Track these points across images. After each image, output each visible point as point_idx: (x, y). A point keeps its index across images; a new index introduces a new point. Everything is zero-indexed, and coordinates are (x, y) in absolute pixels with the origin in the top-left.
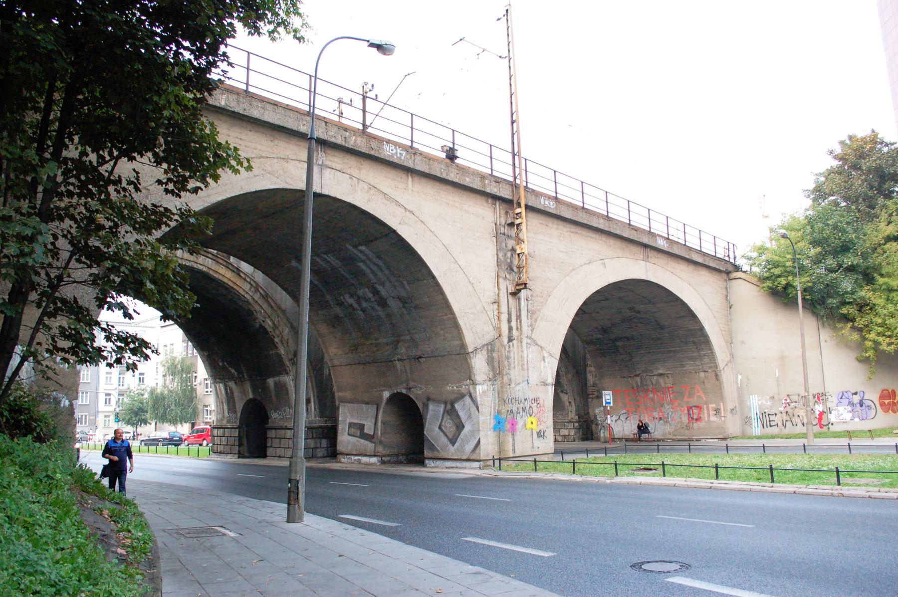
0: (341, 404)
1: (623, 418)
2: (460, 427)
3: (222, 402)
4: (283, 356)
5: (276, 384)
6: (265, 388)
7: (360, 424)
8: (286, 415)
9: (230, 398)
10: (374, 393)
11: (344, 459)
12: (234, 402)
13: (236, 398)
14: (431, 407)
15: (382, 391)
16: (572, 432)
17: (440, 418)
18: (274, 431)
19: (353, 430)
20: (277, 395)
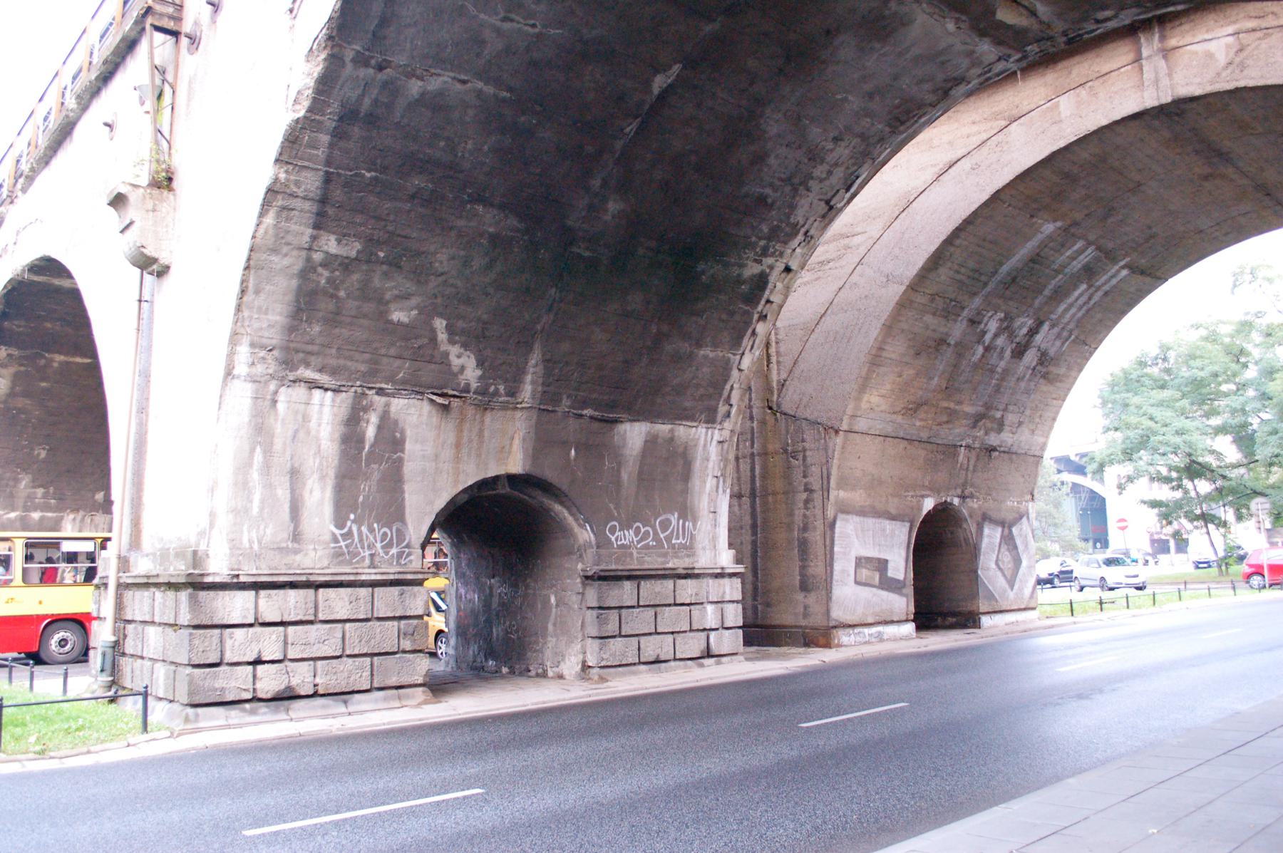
0: (840, 516)
2: (1017, 561)
3: (295, 474)
4: (735, 373)
5: (651, 443)
7: (879, 560)
8: (668, 539)
10: (909, 499)
11: (844, 637)
12: (394, 481)
14: (986, 531)
15: (923, 496)
17: (997, 548)
18: (628, 585)
19: (865, 573)
20: (645, 478)
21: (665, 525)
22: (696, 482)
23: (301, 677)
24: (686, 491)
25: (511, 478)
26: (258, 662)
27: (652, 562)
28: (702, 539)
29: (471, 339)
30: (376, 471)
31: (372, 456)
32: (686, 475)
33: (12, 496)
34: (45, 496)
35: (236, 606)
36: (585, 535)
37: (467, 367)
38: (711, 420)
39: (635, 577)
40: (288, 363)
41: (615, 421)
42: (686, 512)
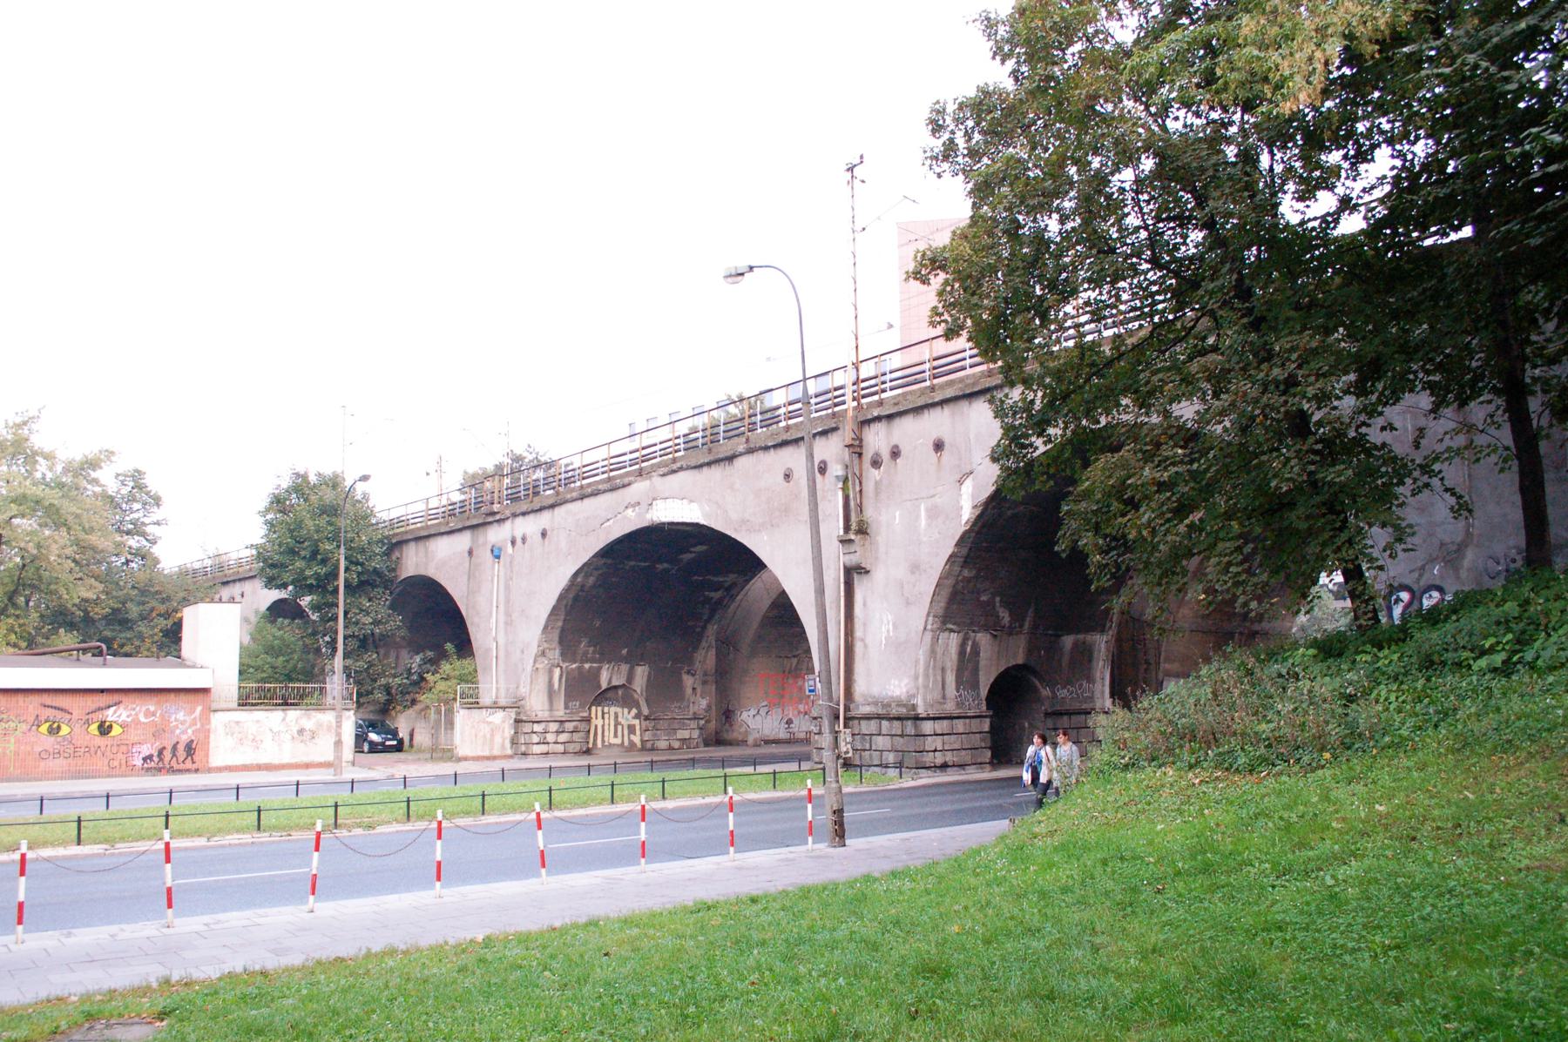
1: (763, 712)
3: (943, 670)
5: (1075, 644)
6: (1053, 648)
9: (967, 663)
12: (976, 670)
13: (982, 663)
16: (696, 734)
18: (1065, 718)
21: (1081, 685)
22: (1094, 663)
23: (949, 758)
24: (1090, 669)
25: (1017, 667)
26: (935, 751)
27: (1076, 706)
28: (1097, 694)
29: (1006, 604)
30: (970, 666)
31: (969, 661)
32: (1090, 661)
33: (574, 653)
34: (594, 652)
35: (928, 727)
36: (1046, 692)
37: (1005, 617)
38: (1103, 632)
39: (1069, 713)
40: (944, 623)
41: (1059, 636)
42: (1090, 679)
